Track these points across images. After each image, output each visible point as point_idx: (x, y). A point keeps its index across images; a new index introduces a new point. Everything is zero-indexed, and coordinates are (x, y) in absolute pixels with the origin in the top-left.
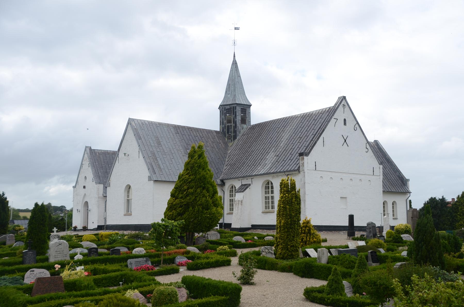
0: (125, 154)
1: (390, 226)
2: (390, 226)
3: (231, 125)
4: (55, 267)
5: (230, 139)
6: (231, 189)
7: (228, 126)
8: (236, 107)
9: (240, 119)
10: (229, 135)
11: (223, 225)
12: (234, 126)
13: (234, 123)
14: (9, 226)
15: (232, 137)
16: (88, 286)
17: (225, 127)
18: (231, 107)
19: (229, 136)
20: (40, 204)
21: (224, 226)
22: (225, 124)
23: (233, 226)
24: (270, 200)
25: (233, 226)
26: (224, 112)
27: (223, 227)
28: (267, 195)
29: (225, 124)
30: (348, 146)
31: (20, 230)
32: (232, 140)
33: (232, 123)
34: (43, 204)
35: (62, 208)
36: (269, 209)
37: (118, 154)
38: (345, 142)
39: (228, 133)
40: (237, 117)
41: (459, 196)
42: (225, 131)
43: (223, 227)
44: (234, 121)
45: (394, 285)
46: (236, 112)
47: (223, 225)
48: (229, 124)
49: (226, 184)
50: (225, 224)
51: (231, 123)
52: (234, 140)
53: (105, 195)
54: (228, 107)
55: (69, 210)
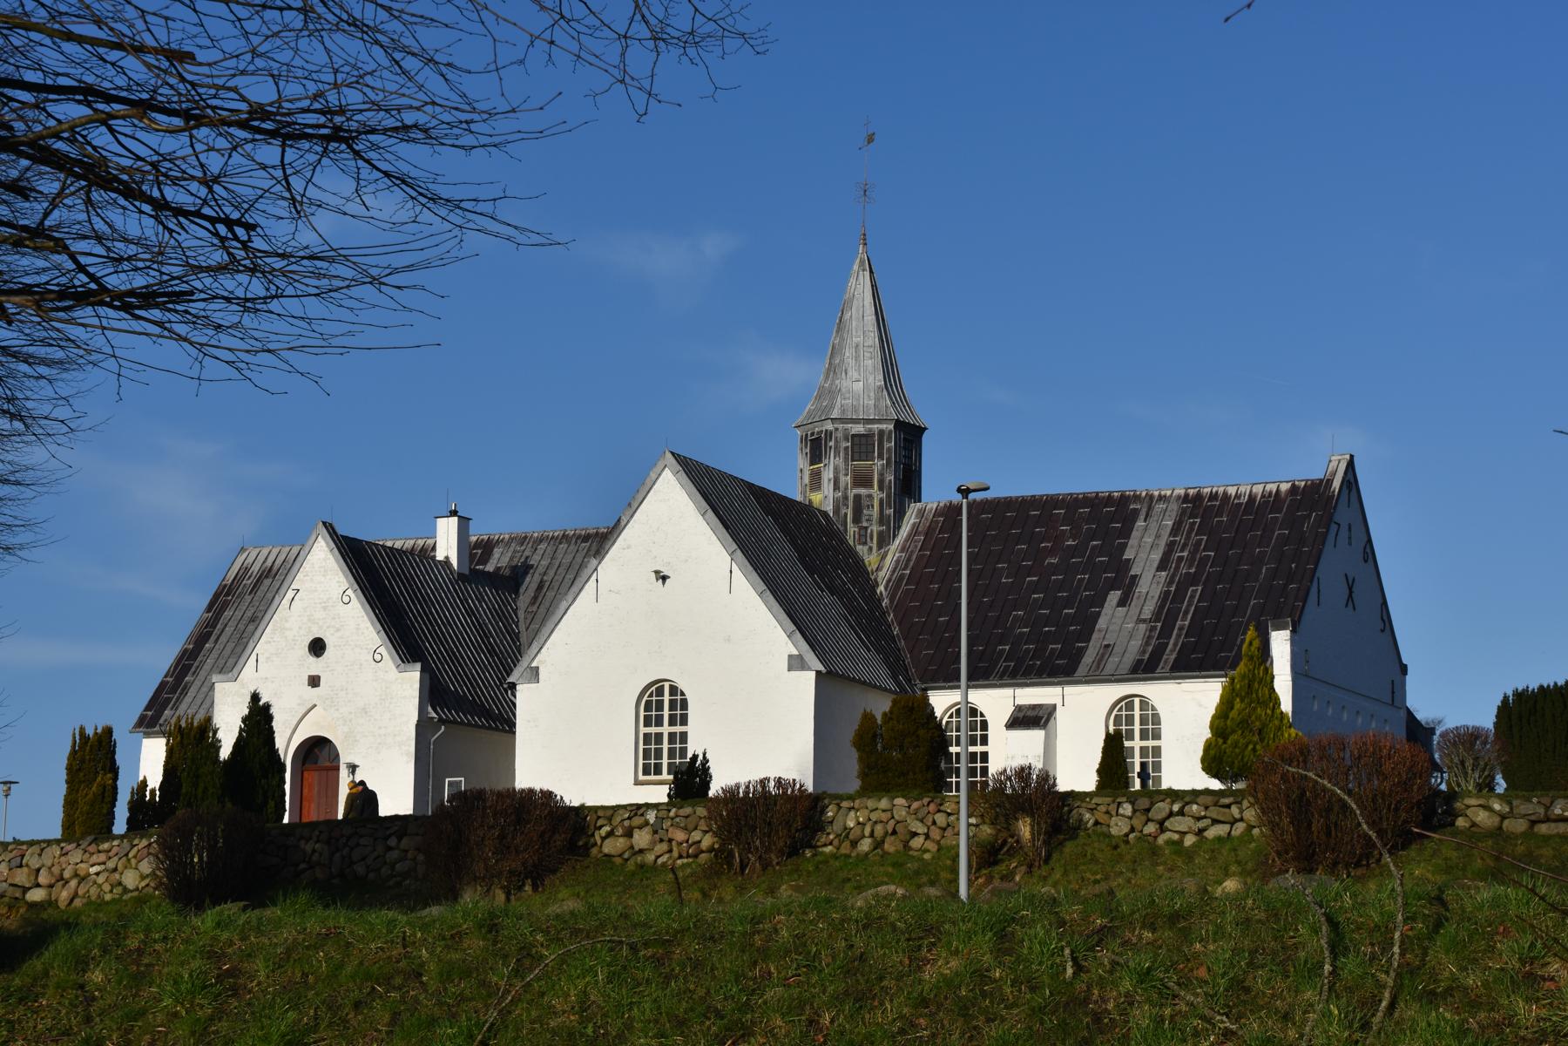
3: (870, 496)
5: (865, 543)
7: (858, 498)
10: (861, 528)
12: (881, 501)
13: (881, 488)
14: (146, 867)
15: (872, 539)
16: (1007, 821)
18: (870, 430)
19: (863, 532)
20: (1520, 689)
22: (846, 489)
28: (678, 729)
29: (846, 489)
34: (1556, 684)
36: (661, 774)
38: (542, 36)
41: (1506, 698)
42: (846, 514)
45: (1300, 734)
48: (863, 491)
51: (871, 486)
54: (859, 429)
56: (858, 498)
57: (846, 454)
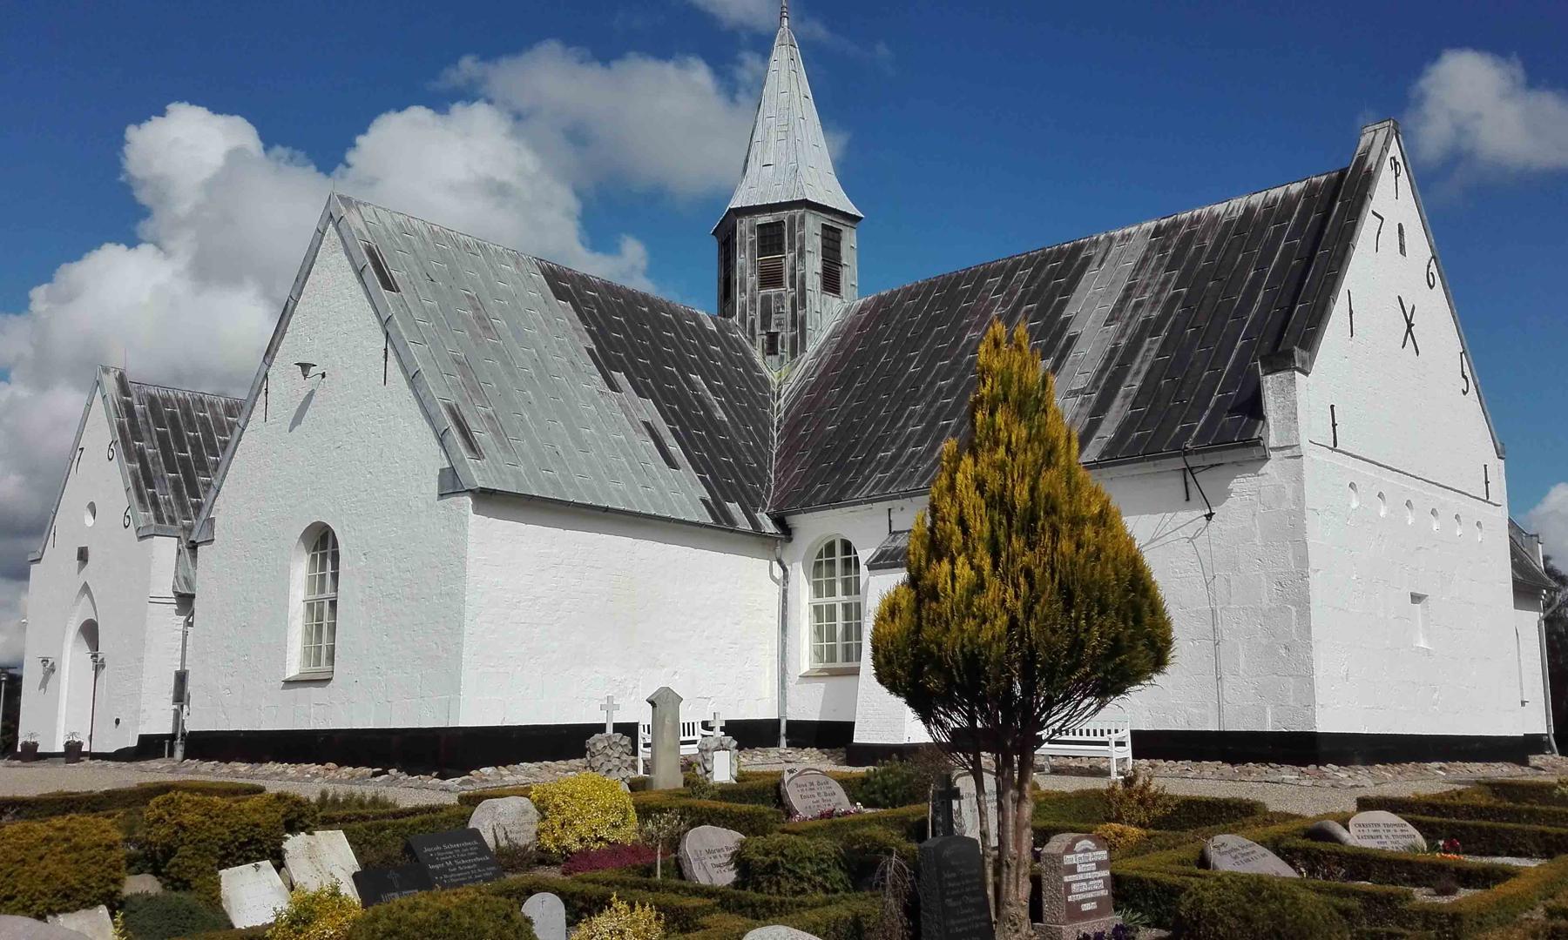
0: (305, 367)
1: (283, 688)
2: (283, 688)
4: (150, 116)
6: (820, 555)
8: (802, 217)
9: (820, 271)
11: (783, 730)
13: (793, 285)
15: (783, 347)
17: (753, 301)
21: (788, 735)
23: (859, 738)
24: (840, 622)
25: (859, 738)
26: (748, 240)
27: (783, 741)
30: (1418, 353)
31: (1346, 174)
32: (782, 358)
33: (788, 285)
35: (748, 863)
37: (266, 375)
39: (765, 324)
40: (808, 257)
43: (783, 741)
44: (793, 277)
46: (802, 239)
47: (783, 730)
48: (773, 291)
49: (797, 536)
50: (789, 723)
52: (793, 354)
53: (186, 591)
54: (763, 219)
55: (151, 876)
56: (766, 300)
57: (752, 249)
